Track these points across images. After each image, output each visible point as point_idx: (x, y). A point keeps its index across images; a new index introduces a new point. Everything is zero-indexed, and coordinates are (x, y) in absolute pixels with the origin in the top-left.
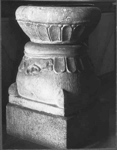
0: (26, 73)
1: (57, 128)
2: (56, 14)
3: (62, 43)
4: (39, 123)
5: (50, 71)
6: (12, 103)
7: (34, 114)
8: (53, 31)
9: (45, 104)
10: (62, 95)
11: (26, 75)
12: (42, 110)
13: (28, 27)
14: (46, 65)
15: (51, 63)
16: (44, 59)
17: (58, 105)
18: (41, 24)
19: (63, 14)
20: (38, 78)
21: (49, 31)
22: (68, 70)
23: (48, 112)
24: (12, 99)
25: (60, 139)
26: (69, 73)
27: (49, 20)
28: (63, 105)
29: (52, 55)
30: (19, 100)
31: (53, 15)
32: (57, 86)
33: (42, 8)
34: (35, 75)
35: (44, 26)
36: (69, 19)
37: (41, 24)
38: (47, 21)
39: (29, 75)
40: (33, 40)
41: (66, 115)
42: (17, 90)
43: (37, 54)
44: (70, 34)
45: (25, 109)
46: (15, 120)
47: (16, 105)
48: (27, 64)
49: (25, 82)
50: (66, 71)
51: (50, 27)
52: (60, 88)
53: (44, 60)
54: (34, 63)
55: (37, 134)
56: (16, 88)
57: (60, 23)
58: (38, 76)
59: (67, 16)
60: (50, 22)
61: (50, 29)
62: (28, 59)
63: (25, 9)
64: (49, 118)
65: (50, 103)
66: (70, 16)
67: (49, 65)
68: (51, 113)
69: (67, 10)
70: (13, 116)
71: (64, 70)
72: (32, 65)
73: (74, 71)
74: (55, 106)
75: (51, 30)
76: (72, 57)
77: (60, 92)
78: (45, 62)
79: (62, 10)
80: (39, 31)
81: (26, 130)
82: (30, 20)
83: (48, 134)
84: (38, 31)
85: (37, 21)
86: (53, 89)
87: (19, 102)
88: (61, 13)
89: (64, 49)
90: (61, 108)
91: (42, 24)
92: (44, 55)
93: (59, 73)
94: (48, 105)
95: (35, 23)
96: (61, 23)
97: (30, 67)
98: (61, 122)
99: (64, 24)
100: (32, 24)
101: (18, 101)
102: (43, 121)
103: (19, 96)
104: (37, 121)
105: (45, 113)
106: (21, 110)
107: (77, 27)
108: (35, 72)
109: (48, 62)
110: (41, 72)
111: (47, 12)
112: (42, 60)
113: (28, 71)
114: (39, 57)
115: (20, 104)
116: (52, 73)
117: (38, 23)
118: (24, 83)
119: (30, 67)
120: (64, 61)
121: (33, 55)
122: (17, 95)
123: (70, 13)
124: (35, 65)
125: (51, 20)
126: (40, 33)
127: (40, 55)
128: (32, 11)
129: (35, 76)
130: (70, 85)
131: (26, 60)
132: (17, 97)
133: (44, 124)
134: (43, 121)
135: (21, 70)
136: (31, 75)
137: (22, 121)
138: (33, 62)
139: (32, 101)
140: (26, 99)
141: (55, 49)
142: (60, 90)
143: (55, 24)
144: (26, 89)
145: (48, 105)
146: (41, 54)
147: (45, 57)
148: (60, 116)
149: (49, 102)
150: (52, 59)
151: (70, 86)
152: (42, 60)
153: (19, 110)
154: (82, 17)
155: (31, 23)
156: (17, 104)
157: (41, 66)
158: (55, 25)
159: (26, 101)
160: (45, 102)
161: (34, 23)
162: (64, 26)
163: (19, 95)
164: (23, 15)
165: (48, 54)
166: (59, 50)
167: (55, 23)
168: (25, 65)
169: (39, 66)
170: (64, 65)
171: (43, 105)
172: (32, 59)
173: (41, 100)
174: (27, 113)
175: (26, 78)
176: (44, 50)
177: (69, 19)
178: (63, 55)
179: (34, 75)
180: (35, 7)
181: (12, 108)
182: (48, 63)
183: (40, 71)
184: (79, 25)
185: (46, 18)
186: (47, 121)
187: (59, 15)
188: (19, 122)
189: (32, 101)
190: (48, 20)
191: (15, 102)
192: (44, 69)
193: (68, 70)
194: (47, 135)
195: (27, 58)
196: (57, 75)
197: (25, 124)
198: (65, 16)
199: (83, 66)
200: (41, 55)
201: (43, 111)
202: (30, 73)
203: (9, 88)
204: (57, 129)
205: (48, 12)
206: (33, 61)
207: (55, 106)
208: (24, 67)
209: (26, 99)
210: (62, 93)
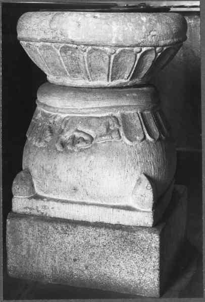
0: (59, 148)
2: (131, 28)
3: (128, 84)
4: (93, 246)
5: (115, 141)
6: (21, 211)
7: (80, 228)
8: (120, 60)
9: (106, 206)
10: (146, 185)
11: (59, 152)
12: (98, 220)
13: (63, 54)
14: (105, 129)
15: (116, 125)
16: (98, 118)
17: (136, 206)
18: (97, 48)
19: (144, 27)
20: (92, 157)
21: (112, 62)
22: (149, 135)
23: (114, 222)
24: (20, 203)
25: (142, 271)
26: (151, 142)
27: (117, 39)
28: (151, 205)
29: (114, 109)
30: (39, 204)
31: (124, 28)
32: (134, 168)
33: (98, 14)
34: (81, 150)
35: (103, 51)
36: (153, 37)
37: (97, 48)
38: (114, 42)
39: (67, 152)
40: (51, 78)
41: (155, 225)
42: (33, 185)
43: (81, 108)
44: (148, 64)
46: (29, 246)
47: (33, 215)
48: (56, 131)
49: (58, 167)
50: (145, 137)
51: (117, 52)
52: (138, 172)
53: (98, 119)
54: (76, 127)
55: (87, 267)
56: (31, 180)
57: (137, 46)
59: (151, 31)
60: (120, 44)
61: (115, 56)
62: (56, 120)
63: (57, 17)
64: (118, 233)
65: (116, 204)
66: (155, 31)
67: (111, 130)
68: (121, 223)
69: (147, 18)
70: (24, 237)
71: (142, 137)
72: (72, 130)
73: (157, 137)
74: (129, 208)
75: (116, 59)
76: (148, 110)
77: (139, 181)
78: (101, 124)
79: (139, 18)
80: (90, 61)
81: (60, 264)
82: (74, 39)
83: (113, 266)
84: (88, 61)
85: (91, 40)
86: (127, 176)
87: (40, 209)
88: (139, 25)
89: (136, 95)
90: (144, 212)
91: (101, 48)
92: (98, 110)
93: (134, 144)
94: (114, 207)
95: (84, 45)
96: (141, 45)
97: (67, 136)
99: (145, 46)
100: (77, 48)
101: (38, 206)
102: (102, 241)
103: (37, 197)
104: (88, 242)
105: (106, 224)
106: (45, 225)
107: (163, 51)
108: (81, 145)
109: (109, 124)
110: (96, 144)
111: (111, 23)
112: (94, 120)
113: (63, 145)
114: (85, 114)
115: (43, 213)
116: (120, 145)
117: (92, 45)
118: (56, 169)
119: (67, 136)
120: (138, 118)
121: (73, 111)
122: (33, 195)
123: (155, 25)
124: (77, 131)
125: (121, 39)
126: (90, 65)
127: (88, 110)
128: (78, 22)
129: (82, 153)
130: (155, 164)
131: (51, 121)
132: (34, 198)
133: (105, 246)
134: (102, 240)
135: (44, 142)
136: (72, 152)
137: (47, 245)
139: (72, 203)
140: (57, 201)
141: (119, 97)
142: (140, 176)
143: (128, 47)
144: (60, 181)
145: (114, 207)
147: (100, 113)
148: (142, 227)
149: (115, 203)
150: (115, 117)
151: (154, 166)
153: (40, 225)
154: (174, 32)
155: (75, 46)
156: (35, 212)
157: (93, 132)
158: (127, 48)
159: (56, 205)
160: (104, 203)
161: (83, 46)
162: (144, 49)
163: (37, 194)
164: (55, 31)
165: (106, 107)
166: (127, 98)
167: (128, 45)
168: (51, 132)
169: (91, 132)
170: (140, 126)
171: (102, 209)
172: (67, 119)
173: (94, 199)
174: (62, 229)
175: (61, 158)
176: (98, 98)
177: (155, 35)
178: (135, 107)
179: (81, 151)
180: (81, 14)
181: (23, 223)
182: (109, 125)
183: (93, 142)
184: (170, 46)
185: (110, 35)
186: (113, 240)
187: (136, 29)
188: (42, 250)
189: (72, 203)
190: (114, 38)
191: (28, 210)
192: (103, 137)
193: (147, 135)
194: (113, 268)
195: (54, 118)
196: (131, 146)
197: (56, 252)
198: (147, 30)
199: (163, 126)
200: (92, 110)
201: (101, 221)
202: (69, 148)
203: (14, 182)
204: (137, 253)
205: (114, 23)
206: (72, 122)
207: (129, 208)
208: (50, 135)
209: (57, 201)
210: (146, 182)
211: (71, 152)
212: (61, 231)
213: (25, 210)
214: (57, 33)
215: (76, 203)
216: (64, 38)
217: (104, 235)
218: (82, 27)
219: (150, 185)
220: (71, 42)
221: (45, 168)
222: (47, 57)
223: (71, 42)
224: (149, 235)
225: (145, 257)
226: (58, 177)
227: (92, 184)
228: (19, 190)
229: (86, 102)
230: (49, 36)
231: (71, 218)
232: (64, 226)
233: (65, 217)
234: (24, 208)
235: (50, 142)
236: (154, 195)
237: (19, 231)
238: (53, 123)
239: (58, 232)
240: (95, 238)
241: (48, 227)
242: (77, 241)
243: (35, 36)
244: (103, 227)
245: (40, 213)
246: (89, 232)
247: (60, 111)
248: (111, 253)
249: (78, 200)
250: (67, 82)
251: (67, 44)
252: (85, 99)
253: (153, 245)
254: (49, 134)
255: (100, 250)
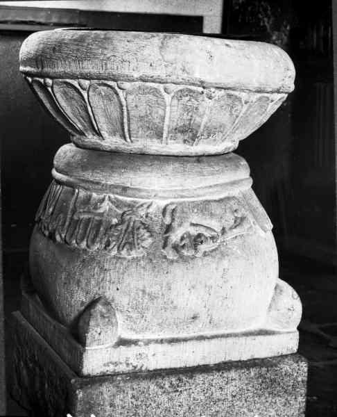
0: (171, 255)
1: (279, 391)
7: (200, 378)
9: (236, 335)
11: (172, 262)
13: (175, 101)
20: (225, 263)
45: (156, 374)
58: (219, 256)
62: (150, 210)
90: (288, 333)
98: (290, 370)
102: (232, 389)
106: (144, 384)
113: (176, 248)
115: (135, 367)
117: (228, 89)
134: (231, 389)
136: (193, 258)
138: (182, 215)
139: (185, 340)
146: (208, 185)
147: (220, 192)
152: (214, 205)
156: (122, 368)
161: (213, 90)
164: (172, 64)
165: (227, 184)
168: (148, 229)
171: (230, 340)
174: (172, 385)
175: (178, 270)
181: (106, 390)
189: (185, 340)
195: (148, 207)
200: (211, 190)
204: (279, 396)
211: (192, 259)
212: (170, 390)
213: (107, 368)
214: (175, 68)
215: (191, 339)
216: (186, 75)
217: (235, 379)
218: (215, 59)
219: (295, 293)
220: (198, 83)
221: (148, 290)
222: (136, 106)
223: (198, 83)
224: (295, 365)
225: (289, 398)
226: (172, 302)
227: (225, 304)
228: (102, 335)
229: (202, 177)
230: (160, 72)
231: (183, 365)
232: (173, 379)
233: (173, 366)
234: (104, 365)
235: (150, 247)
236: (303, 307)
237: (99, 405)
238: (147, 216)
239: (164, 392)
240: (221, 388)
241: (149, 387)
242: (194, 399)
243: (126, 72)
244: (231, 368)
245: (131, 368)
246: (212, 380)
247: (160, 195)
248: (243, 404)
249: (192, 335)
250: (153, 148)
251: (189, 87)
252: (201, 174)
253: (300, 379)
254: (147, 234)
255: (227, 404)
